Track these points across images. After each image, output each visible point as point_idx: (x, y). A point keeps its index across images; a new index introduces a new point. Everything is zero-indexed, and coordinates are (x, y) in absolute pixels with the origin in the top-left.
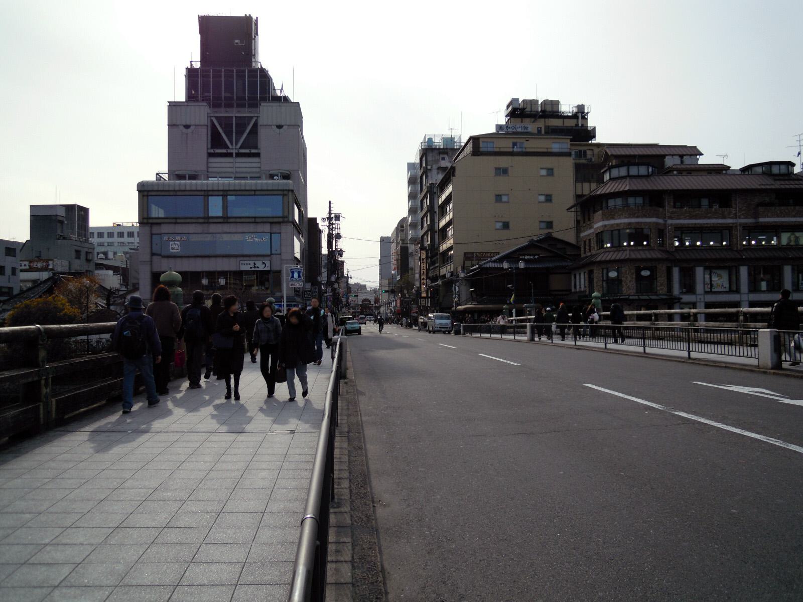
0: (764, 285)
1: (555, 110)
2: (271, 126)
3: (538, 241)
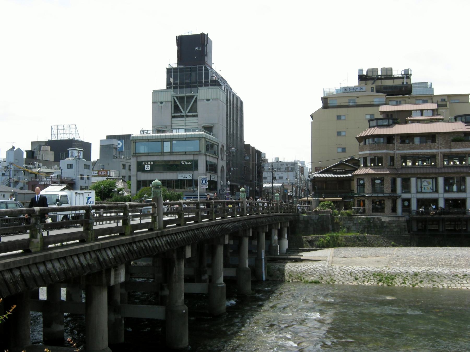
0: (455, 188)
1: (389, 74)
2: (204, 100)
3: (346, 161)
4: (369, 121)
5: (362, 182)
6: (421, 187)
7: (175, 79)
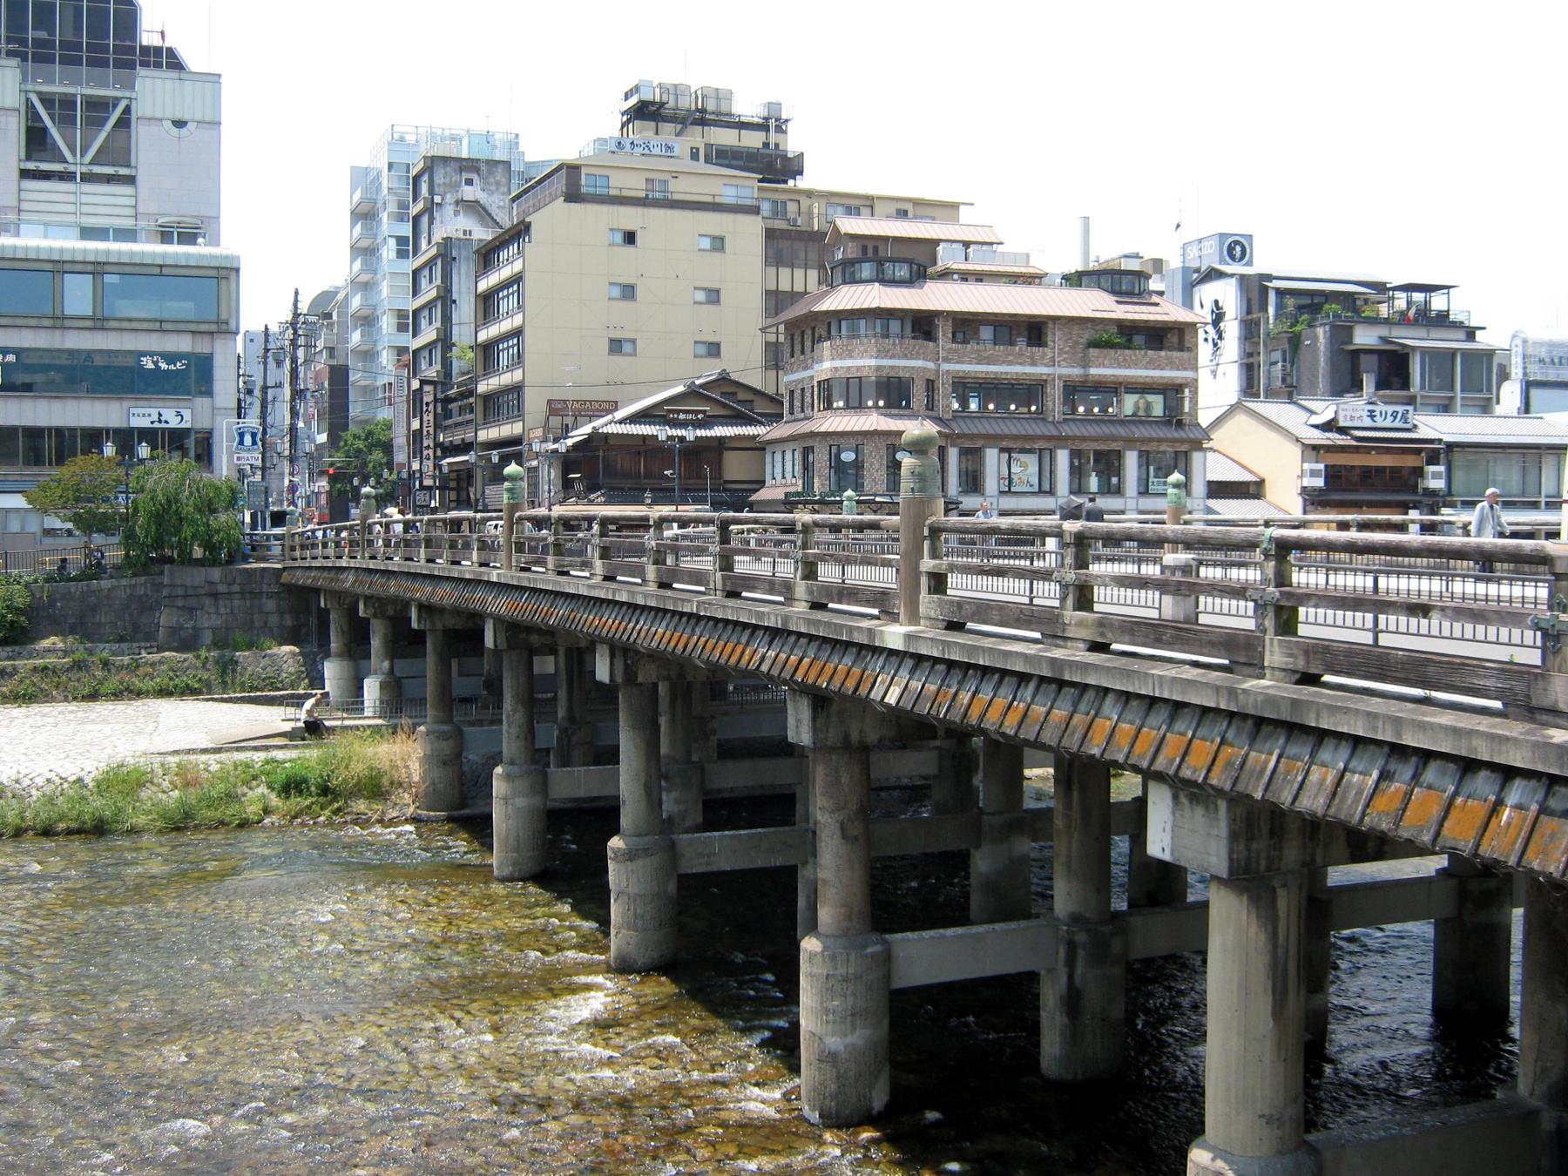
1: (724, 109)
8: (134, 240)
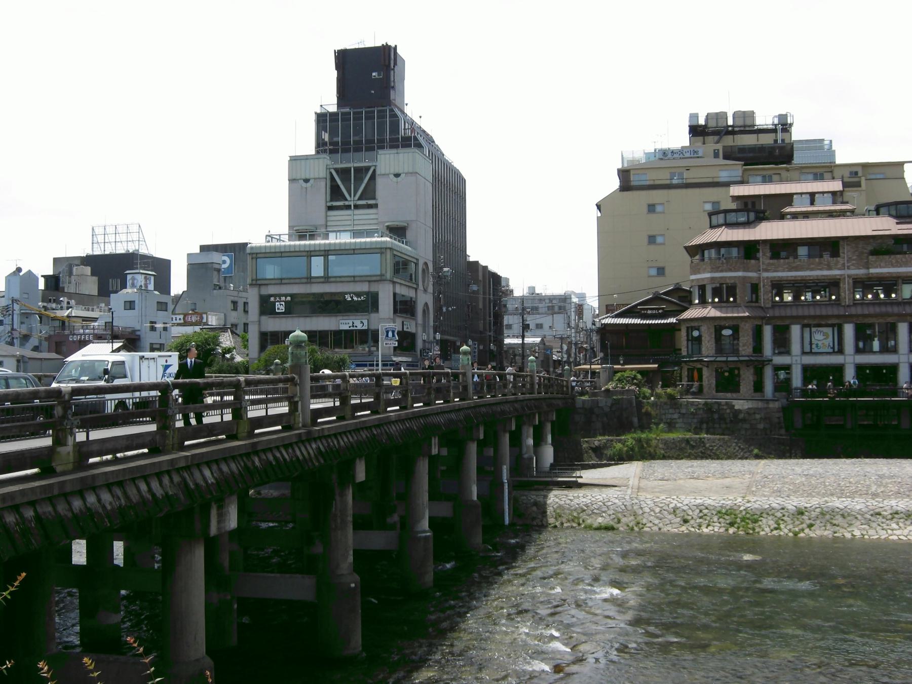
1: (748, 123)
4: (711, 214)
5: (696, 334)
6: (811, 344)
7: (333, 133)
8: (312, 237)
